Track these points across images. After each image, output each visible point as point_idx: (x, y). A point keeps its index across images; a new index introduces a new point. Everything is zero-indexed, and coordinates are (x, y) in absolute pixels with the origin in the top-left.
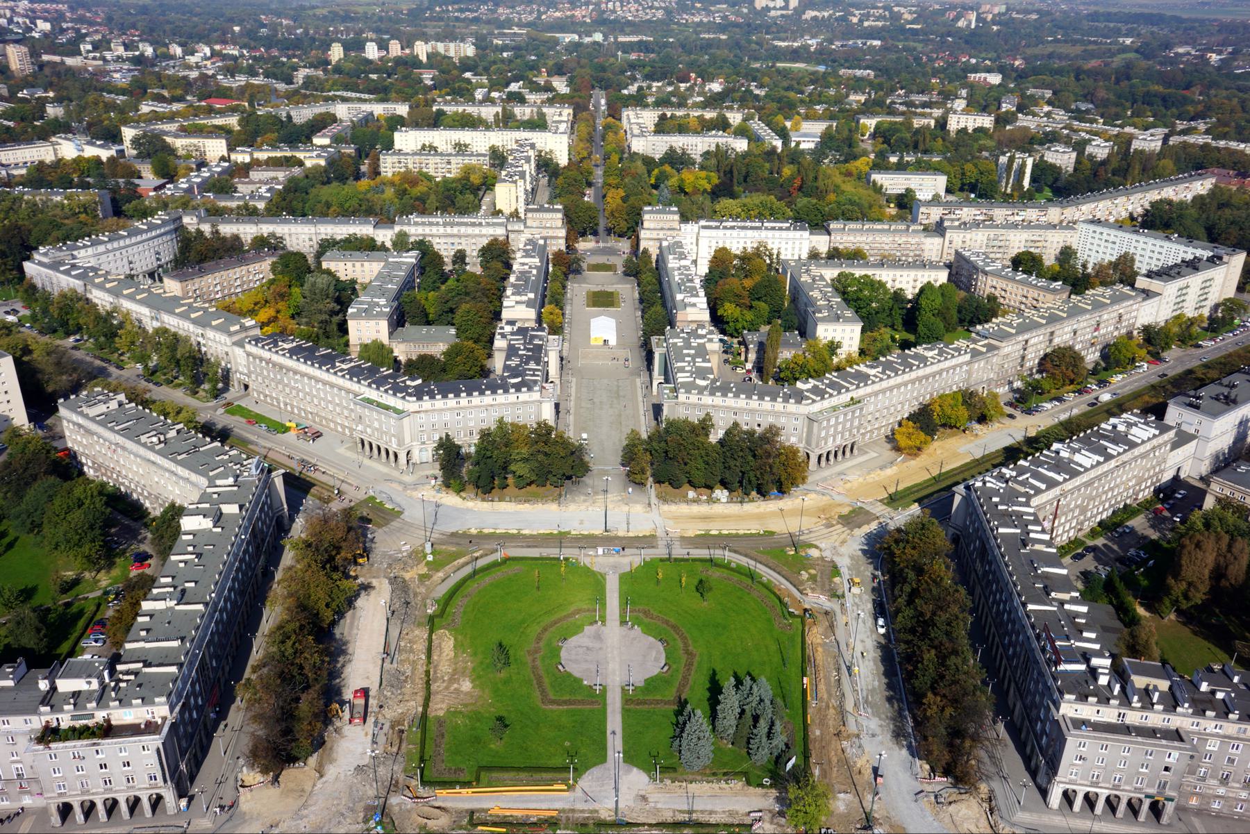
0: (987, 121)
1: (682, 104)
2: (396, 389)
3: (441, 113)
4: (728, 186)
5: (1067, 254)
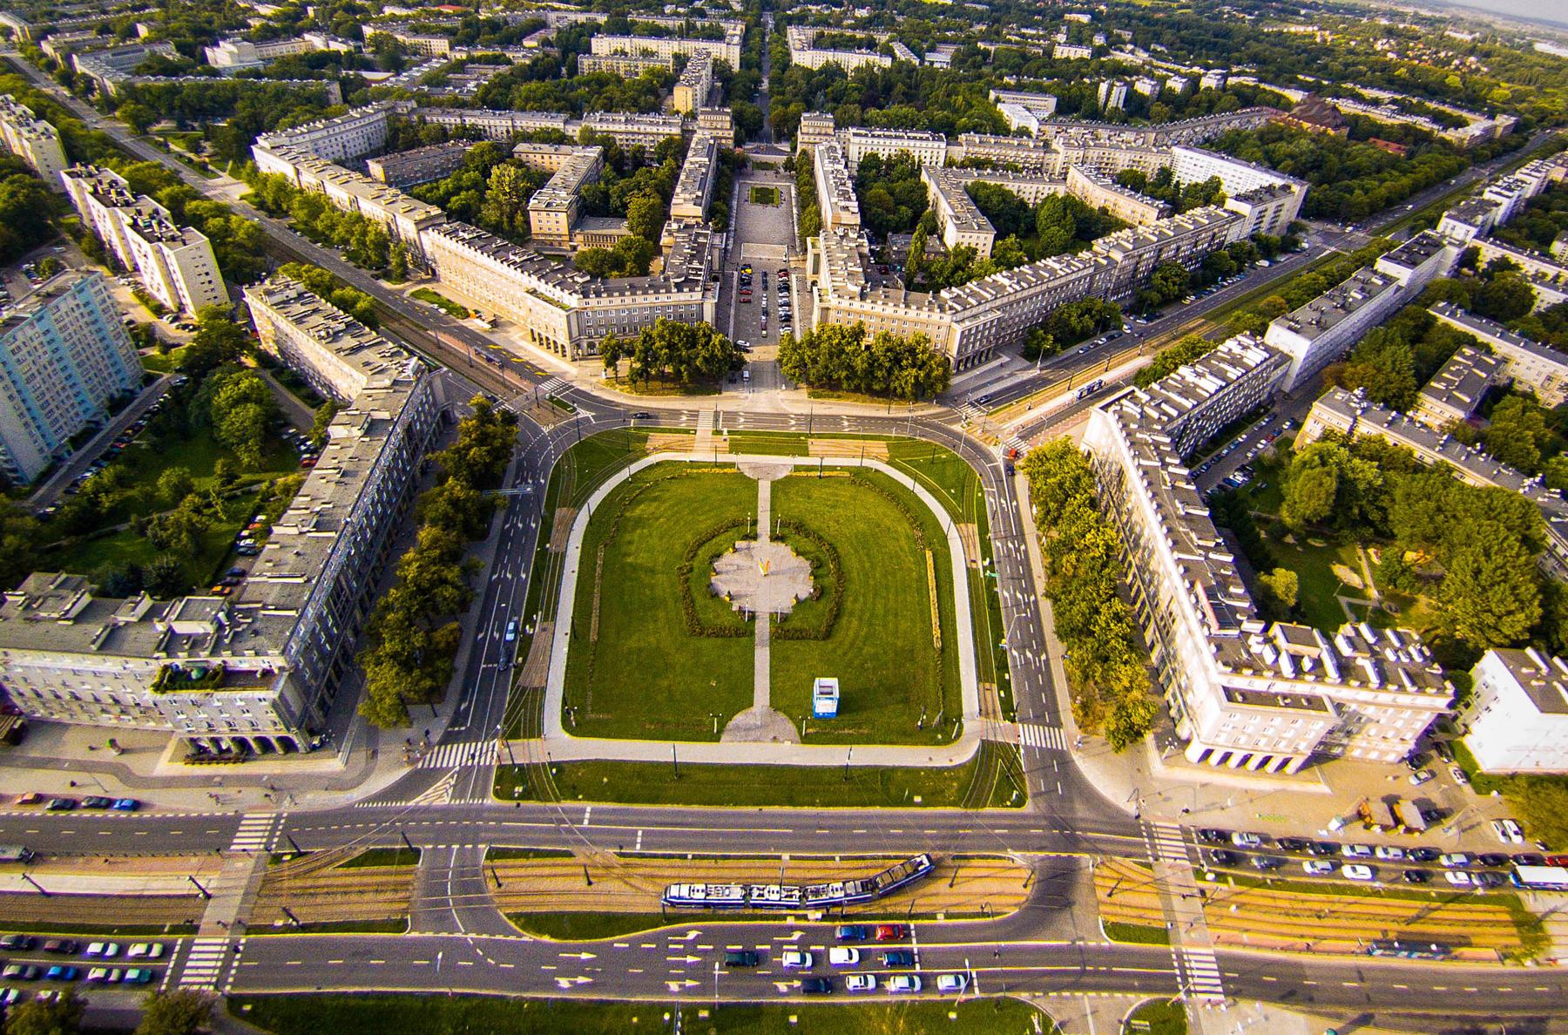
0: (1085, 53)
1: (838, 25)
2: (561, 284)
3: (634, 23)
4: (868, 101)
5: (1165, 175)
